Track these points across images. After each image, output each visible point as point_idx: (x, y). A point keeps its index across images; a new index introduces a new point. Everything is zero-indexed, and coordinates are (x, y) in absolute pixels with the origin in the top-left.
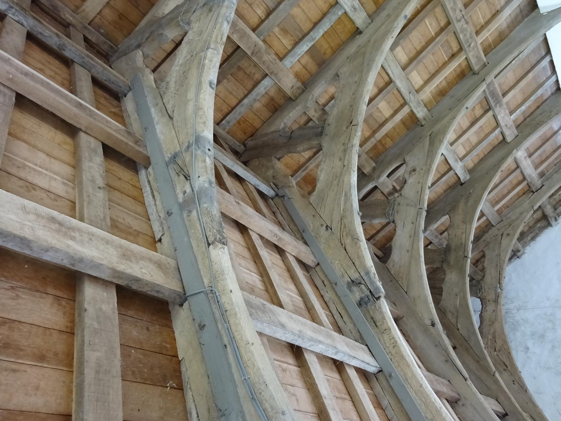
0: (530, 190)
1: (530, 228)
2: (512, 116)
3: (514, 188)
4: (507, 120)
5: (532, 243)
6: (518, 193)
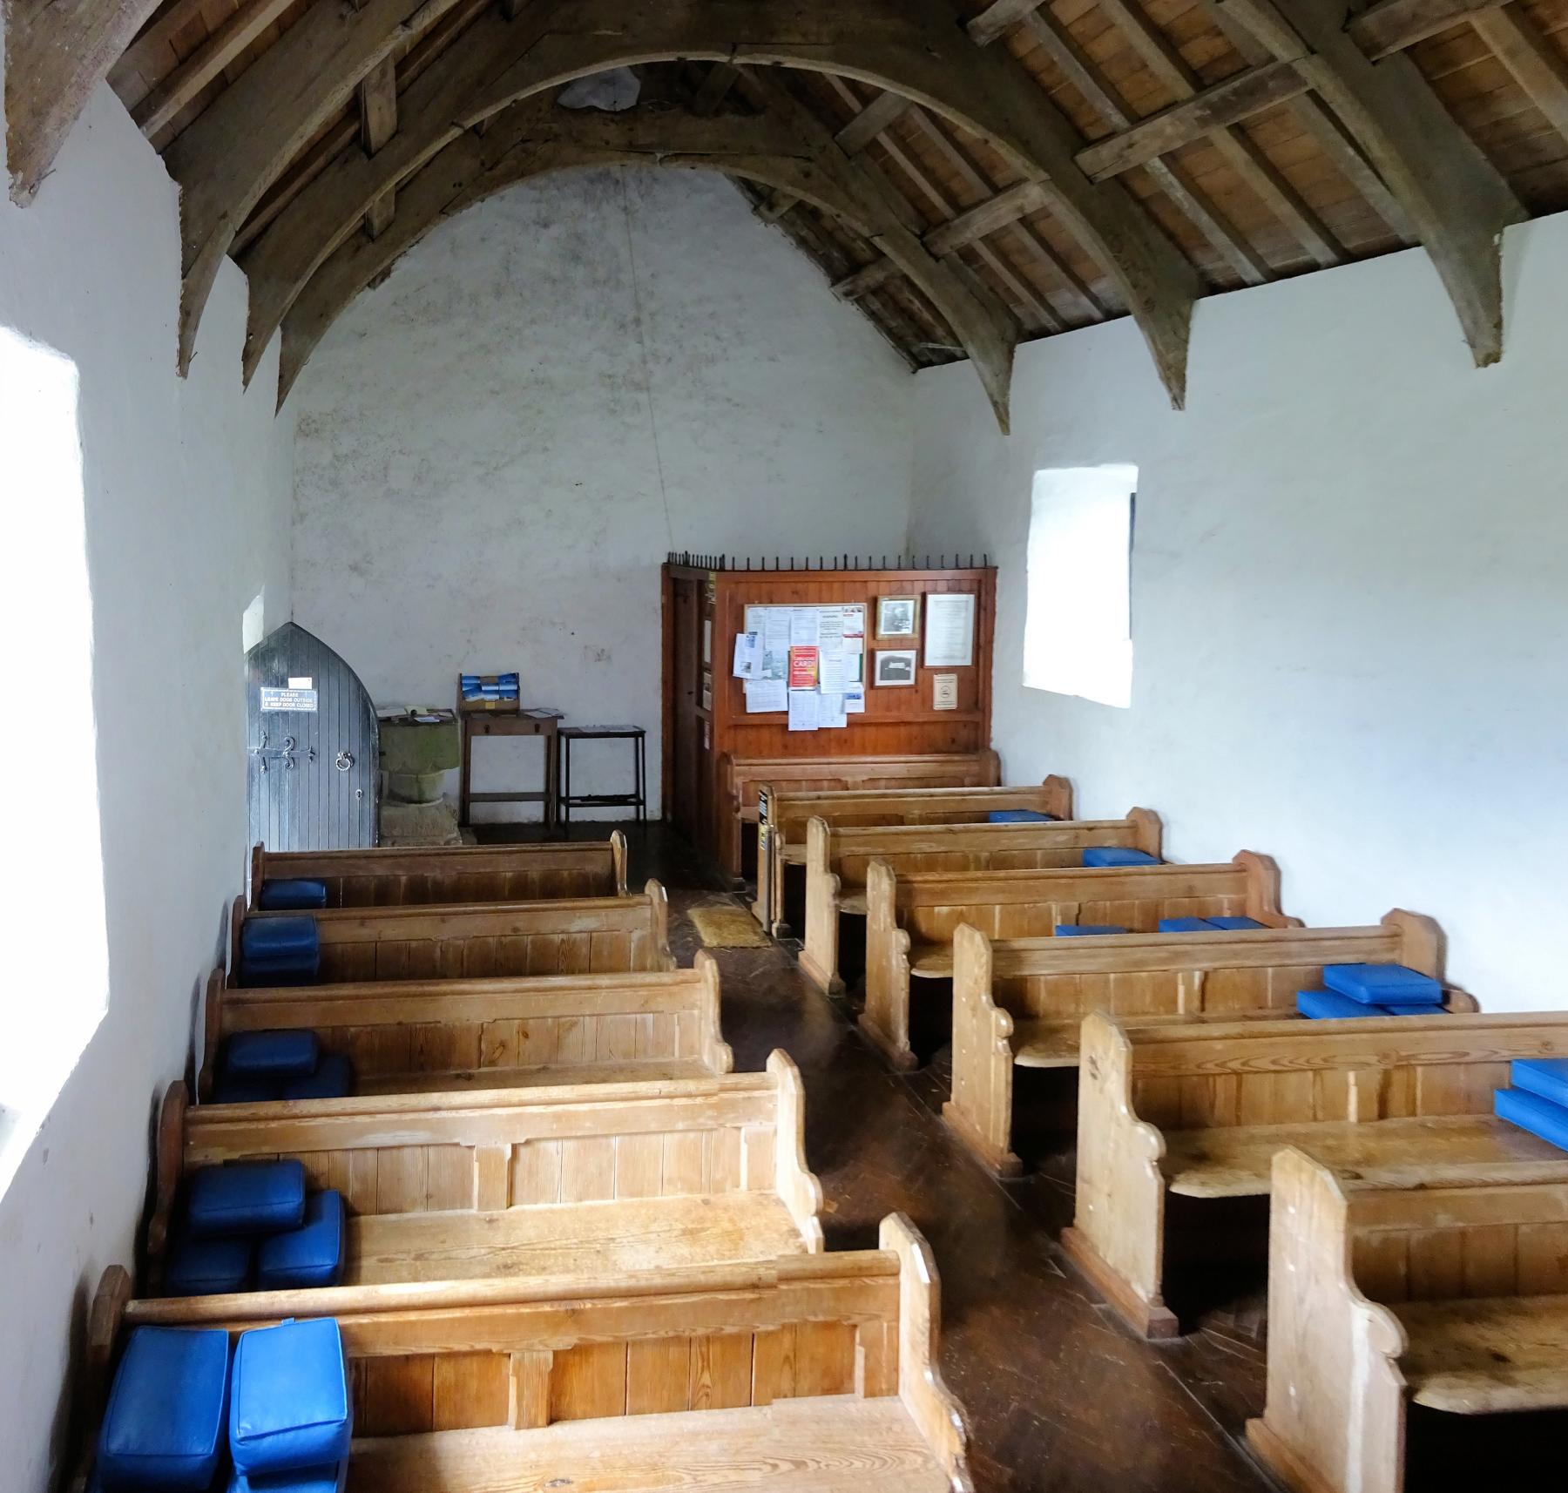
0: (928, 225)
1: (830, 234)
2: (1157, 163)
3: (937, 184)
4: (1147, 148)
5: (790, 239)
6: (924, 195)
